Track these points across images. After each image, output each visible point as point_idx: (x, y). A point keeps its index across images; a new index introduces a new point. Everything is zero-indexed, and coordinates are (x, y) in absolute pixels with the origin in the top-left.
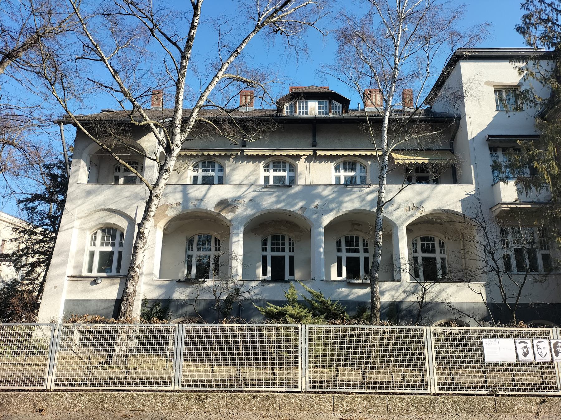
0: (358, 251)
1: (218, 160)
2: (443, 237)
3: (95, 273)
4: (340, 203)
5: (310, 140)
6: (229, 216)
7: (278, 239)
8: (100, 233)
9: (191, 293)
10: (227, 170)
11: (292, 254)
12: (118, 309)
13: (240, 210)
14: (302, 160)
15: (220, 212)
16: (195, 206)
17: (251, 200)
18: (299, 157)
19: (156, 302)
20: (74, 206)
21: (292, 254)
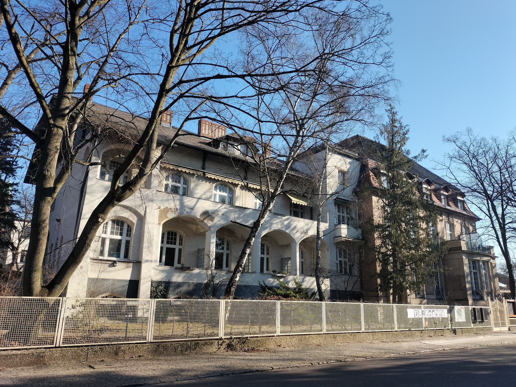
0: (175, 244)
1: (185, 175)
2: (184, 235)
3: (106, 257)
4: (272, 224)
5: (242, 175)
6: (210, 223)
7: (172, 235)
8: (110, 223)
9: (184, 277)
10: (192, 185)
11: (181, 247)
12: (133, 288)
14: (238, 188)
15: (204, 219)
16: (187, 213)
17: (223, 214)
18: (236, 185)
19: (159, 283)
20: (94, 198)
21: (181, 247)
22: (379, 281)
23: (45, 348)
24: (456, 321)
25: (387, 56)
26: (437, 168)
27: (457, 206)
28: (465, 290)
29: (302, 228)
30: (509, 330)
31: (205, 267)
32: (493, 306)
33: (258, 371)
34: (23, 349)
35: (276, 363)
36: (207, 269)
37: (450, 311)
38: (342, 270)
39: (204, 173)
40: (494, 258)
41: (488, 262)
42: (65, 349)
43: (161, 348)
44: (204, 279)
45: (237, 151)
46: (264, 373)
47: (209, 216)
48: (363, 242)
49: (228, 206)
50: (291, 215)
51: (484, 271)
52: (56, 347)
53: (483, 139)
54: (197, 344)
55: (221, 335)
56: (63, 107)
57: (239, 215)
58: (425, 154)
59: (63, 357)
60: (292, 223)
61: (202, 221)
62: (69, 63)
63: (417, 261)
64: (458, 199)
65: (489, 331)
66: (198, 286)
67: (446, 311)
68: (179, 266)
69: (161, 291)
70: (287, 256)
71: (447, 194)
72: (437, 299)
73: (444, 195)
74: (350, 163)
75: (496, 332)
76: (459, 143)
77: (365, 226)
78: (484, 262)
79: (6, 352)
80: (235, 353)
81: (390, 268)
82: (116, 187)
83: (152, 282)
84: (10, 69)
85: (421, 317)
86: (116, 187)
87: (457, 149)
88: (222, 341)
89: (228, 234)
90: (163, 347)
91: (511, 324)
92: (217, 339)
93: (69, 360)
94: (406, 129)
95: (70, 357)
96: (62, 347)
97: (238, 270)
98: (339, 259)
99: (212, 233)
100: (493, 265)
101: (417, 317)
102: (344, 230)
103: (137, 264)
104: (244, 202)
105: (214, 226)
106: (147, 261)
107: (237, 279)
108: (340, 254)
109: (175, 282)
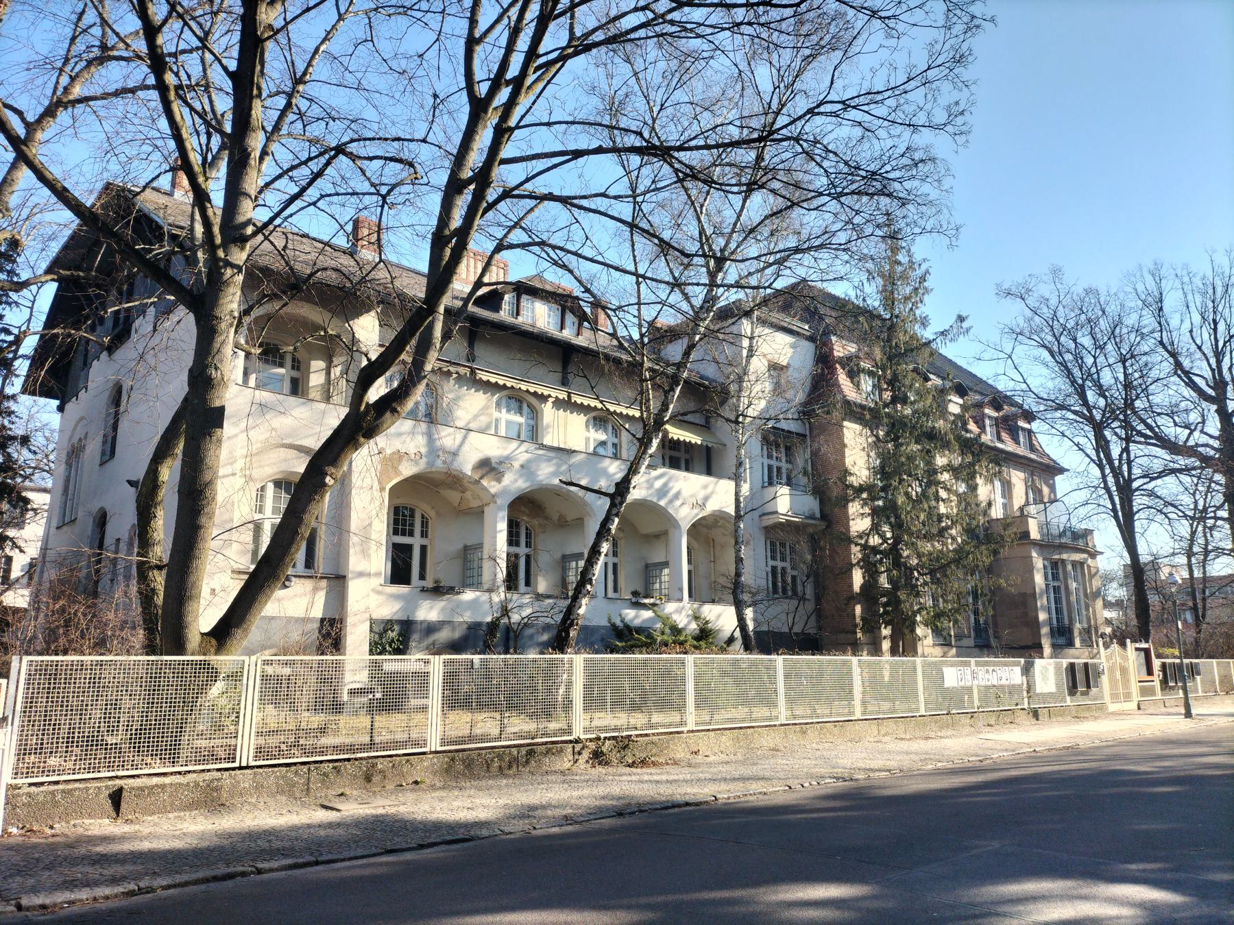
0: (411, 534)
2: (431, 513)
5: (558, 376)
6: (492, 486)
8: (271, 486)
9: (443, 609)
11: (425, 542)
13: (508, 479)
14: (549, 404)
15: (481, 478)
17: (522, 466)
18: (543, 398)
19: (388, 624)
21: (425, 542)
22: (858, 609)
23: (219, 770)
24: (1038, 690)
25: (955, 112)
26: (986, 356)
27: (1017, 442)
28: (1036, 625)
29: (694, 495)
30: (1139, 708)
31: (486, 587)
32: (1108, 658)
33: (687, 804)
34: (172, 774)
35: (724, 786)
36: (490, 591)
37: (1027, 670)
38: (779, 587)
39: (473, 371)
40: (1093, 555)
41: (1082, 564)
42: (261, 770)
43: (464, 764)
44: (486, 614)
45: (540, 316)
46: (704, 807)
47: (493, 469)
48: (823, 525)
49: (532, 447)
50: (664, 465)
51: (1074, 585)
52: (241, 768)
53: (1088, 292)
54: (531, 753)
55: (578, 733)
56: (241, 219)
57: (559, 466)
58: (965, 325)
59: (259, 787)
60: (671, 485)
61: (478, 482)
62: (249, 115)
63: (948, 564)
64: (1019, 427)
65: (1100, 710)
66: (474, 627)
67: (1018, 670)
68: (429, 583)
69: (393, 641)
70: (658, 558)
71: (995, 414)
72: (976, 646)
73: (990, 417)
74: (793, 346)
75: (1113, 714)
76: (1031, 301)
77: (828, 491)
78: (1074, 563)
79: (138, 780)
80: (610, 769)
81: (884, 581)
82: (363, 408)
83: (372, 622)
84: (31, 118)
85: (969, 684)
86: (363, 408)
87: (1029, 313)
88: (580, 745)
89: (529, 512)
90: (463, 761)
91: (1142, 696)
92: (571, 742)
93: (272, 795)
94: (924, 267)
95: (274, 789)
96: (253, 767)
97: (584, 591)
98: (771, 563)
99: (500, 509)
100: (1093, 571)
101: (962, 684)
102: (784, 502)
103: (338, 580)
104: (562, 437)
105: (505, 491)
106: (361, 574)
107: (581, 611)
108: (773, 551)
109: (422, 622)
